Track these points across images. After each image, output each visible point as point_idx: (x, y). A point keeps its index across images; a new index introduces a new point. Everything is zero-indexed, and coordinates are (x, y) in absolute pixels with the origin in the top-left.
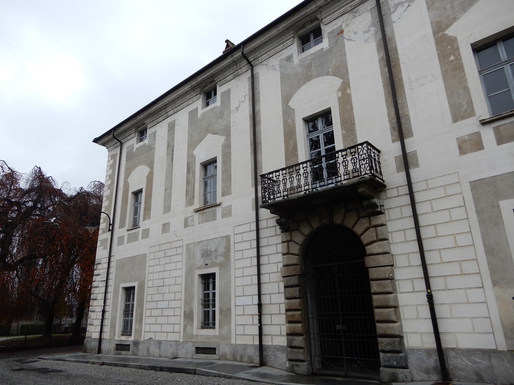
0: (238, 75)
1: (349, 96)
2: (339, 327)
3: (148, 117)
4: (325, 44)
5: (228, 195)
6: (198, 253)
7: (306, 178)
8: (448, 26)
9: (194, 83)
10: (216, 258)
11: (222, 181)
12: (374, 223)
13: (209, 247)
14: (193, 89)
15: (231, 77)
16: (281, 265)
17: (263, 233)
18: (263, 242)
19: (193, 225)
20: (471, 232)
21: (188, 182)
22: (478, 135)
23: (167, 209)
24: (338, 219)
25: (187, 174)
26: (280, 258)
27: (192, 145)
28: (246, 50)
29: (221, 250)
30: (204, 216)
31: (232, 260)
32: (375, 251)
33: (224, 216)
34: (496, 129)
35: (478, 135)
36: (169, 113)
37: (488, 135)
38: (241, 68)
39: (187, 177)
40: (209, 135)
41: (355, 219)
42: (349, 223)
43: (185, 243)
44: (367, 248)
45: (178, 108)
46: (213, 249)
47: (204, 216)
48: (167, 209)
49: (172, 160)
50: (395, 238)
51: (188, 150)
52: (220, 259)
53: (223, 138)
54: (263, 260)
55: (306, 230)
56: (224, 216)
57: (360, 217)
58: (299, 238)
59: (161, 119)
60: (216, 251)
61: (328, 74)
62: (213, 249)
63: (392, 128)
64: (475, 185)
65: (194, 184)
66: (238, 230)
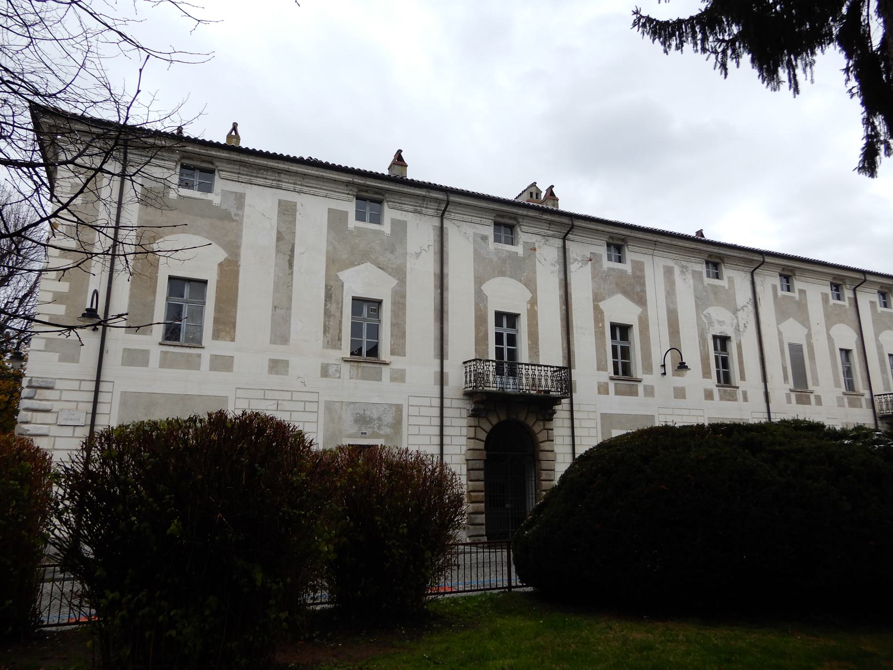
0: (420, 213)
1: (536, 312)
2: (507, 506)
3: (229, 161)
4: (519, 249)
5: (400, 355)
6: (348, 417)
7: (546, 380)
8: (601, 301)
9: (358, 180)
10: (379, 428)
11: (392, 335)
12: (547, 427)
13: (368, 413)
14: (348, 184)
15: (411, 208)
16: (464, 449)
17: (446, 412)
18: (446, 422)
19: (339, 377)
20: (304, 411)
21: (327, 314)
22: (607, 383)
23: (281, 335)
24: (522, 418)
25: (326, 300)
26: (463, 441)
27: (334, 264)
28: (453, 198)
29: (389, 419)
30: (360, 371)
31: (405, 434)
32: (547, 449)
33: (393, 379)
34: (616, 384)
35: (607, 383)
36: (284, 185)
37: (612, 385)
38: (427, 208)
39: (326, 305)
40: (369, 264)
41: (535, 420)
42: (530, 422)
43: (322, 399)
44: (542, 445)
45: (305, 189)
46: (375, 416)
47: (360, 371)
48: (281, 335)
49: (291, 265)
50: (558, 441)
51: (327, 267)
52: (386, 430)
53: (394, 282)
54: (446, 440)
55: (495, 421)
56: (393, 379)
57: (538, 420)
58: (488, 427)
59: (261, 181)
60: (379, 419)
61: (520, 281)
62: (375, 416)
63: (564, 357)
64: (604, 416)
65: (341, 322)
66: (413, 401)
